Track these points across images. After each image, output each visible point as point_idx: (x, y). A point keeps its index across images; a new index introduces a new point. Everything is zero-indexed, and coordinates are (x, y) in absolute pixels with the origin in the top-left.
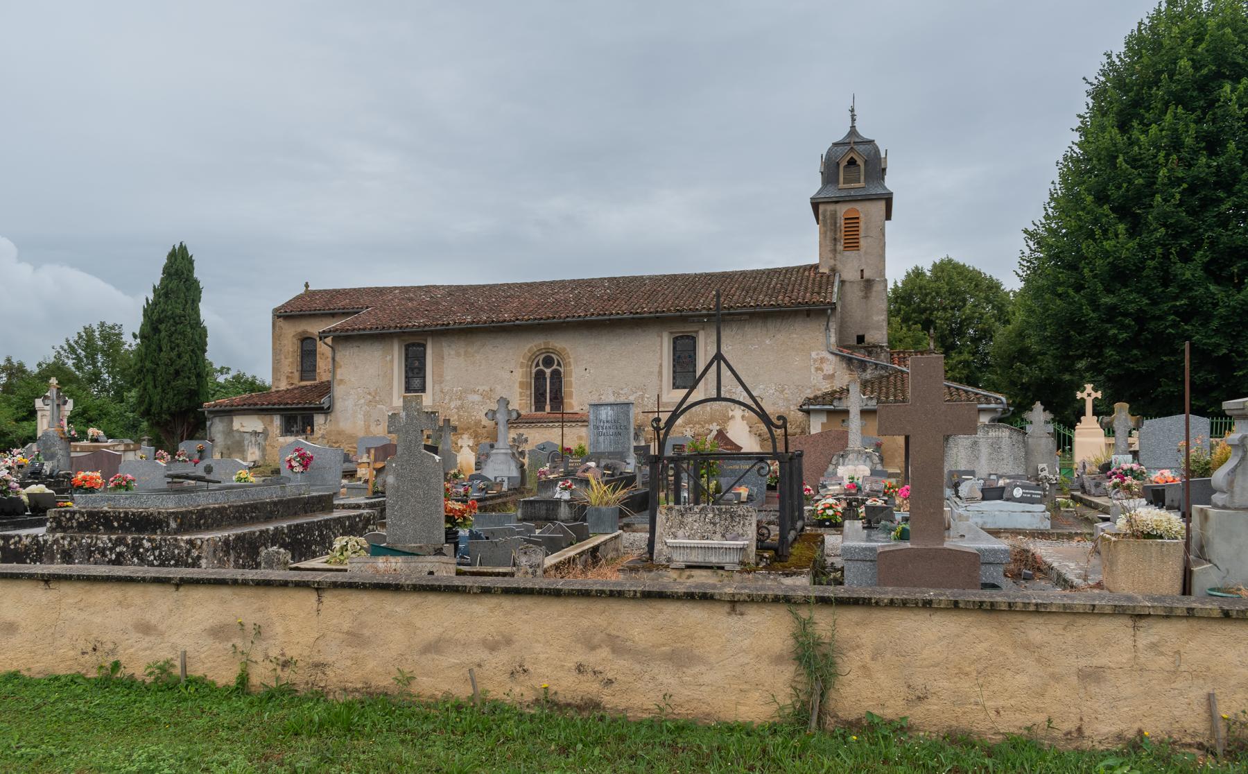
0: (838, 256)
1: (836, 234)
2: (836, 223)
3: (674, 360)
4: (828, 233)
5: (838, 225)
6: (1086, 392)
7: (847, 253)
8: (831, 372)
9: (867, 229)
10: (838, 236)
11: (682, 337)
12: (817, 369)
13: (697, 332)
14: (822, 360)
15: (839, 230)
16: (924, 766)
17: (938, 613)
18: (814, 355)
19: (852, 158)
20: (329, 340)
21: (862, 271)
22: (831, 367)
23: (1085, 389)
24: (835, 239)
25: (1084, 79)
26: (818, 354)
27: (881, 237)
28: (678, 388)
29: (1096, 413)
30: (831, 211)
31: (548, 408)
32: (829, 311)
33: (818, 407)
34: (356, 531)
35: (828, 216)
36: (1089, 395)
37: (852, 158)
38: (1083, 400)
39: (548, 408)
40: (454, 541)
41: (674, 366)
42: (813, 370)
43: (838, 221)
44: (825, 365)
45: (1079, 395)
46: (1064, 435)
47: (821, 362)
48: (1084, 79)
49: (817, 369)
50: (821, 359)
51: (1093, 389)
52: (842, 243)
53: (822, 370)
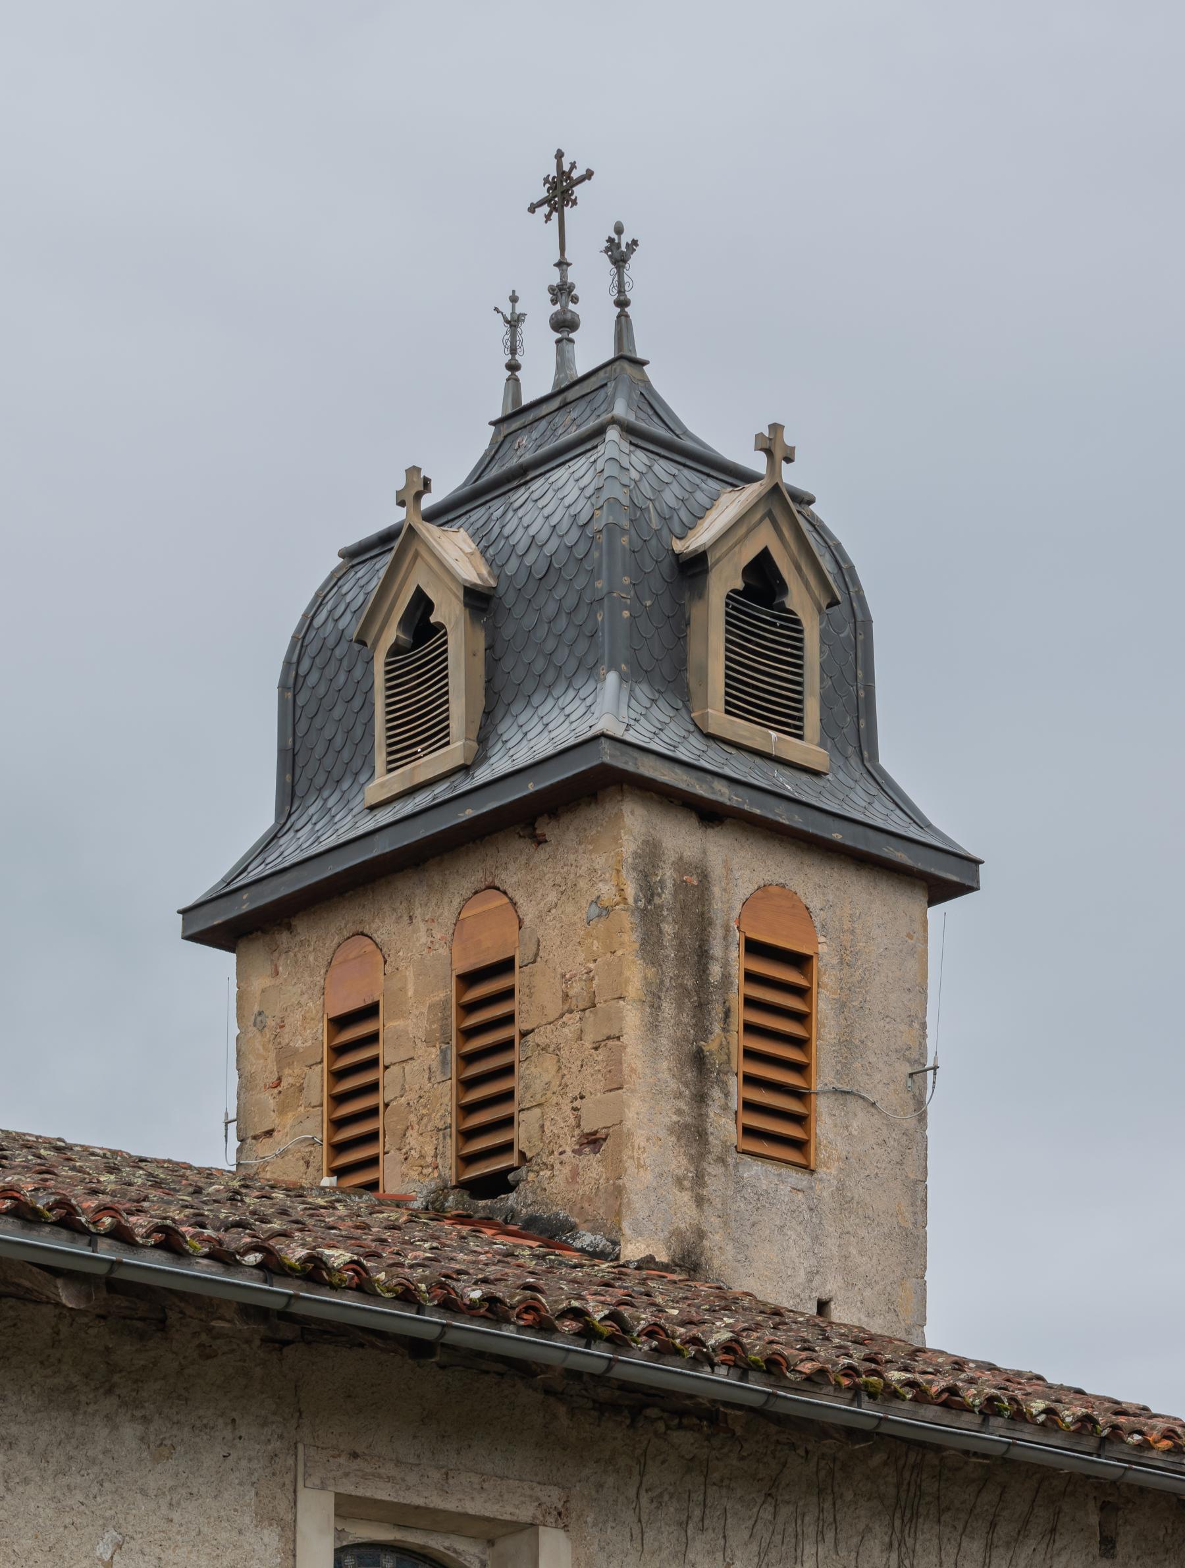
0: (716, 1182)
1: (703, 1031)
2: (703, 956)
4: (668, 1008)
5: (715, 970)
7: (754, 1170)
9: (848, 1046)
10: (711, 1046)
15: (717, 1010)
16: (158, 1184)
17: (300, 925)
24: (699, 1060)
25: (496, 309)
27: (910, 1123)
30: (681, 865)
34: (568, 190)
35: (667, 896)
43: (717, 950)
48: (496, 309)
52: (735, 1104)
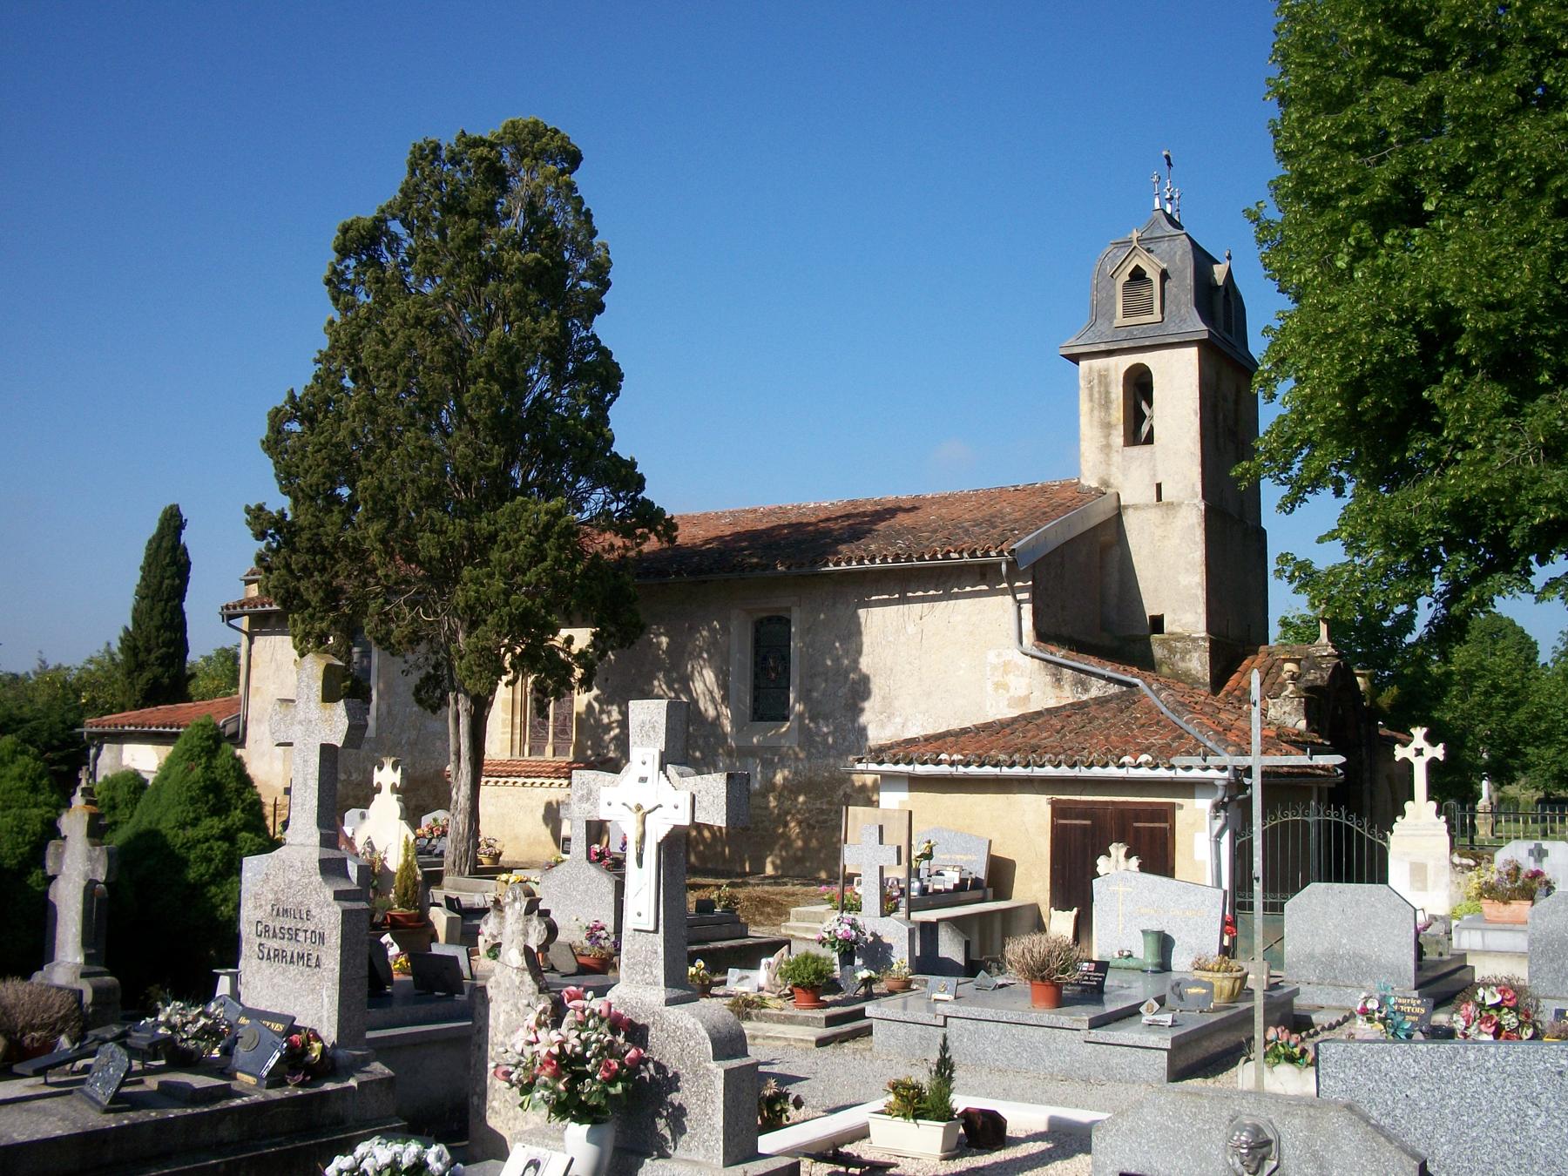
3: (756, 664)
6: (1412, 746)
8: (1023, 692)
11: (769, 619)
12: (998, 686)
13: (788, 610)
14: (1006, 667)
18: (992, 657)
19: (1137, 266)
20: (244, 623)
21: (1159, 486)
22: (1024, 681)
23: (1434, 744)
26: (999, 655)
28: (761, 719)
29: (1434, 792)
31: (549, 750)
32: (927, 557)
33: (988, 770)
36: (1419, 752)
37: (1137, 266)
38: (1406, 762)
39: (549, 750)
40: (1430, 974)
41: (756, 676)
42: (990, 688)
44: (1011, 676)
45: (1400, 753)
46: (1371, 842)
47: (1006, 673)
49: (998, 686)
50: (1006, 664)
51: (1428, 738)
53: (1006, 687)
